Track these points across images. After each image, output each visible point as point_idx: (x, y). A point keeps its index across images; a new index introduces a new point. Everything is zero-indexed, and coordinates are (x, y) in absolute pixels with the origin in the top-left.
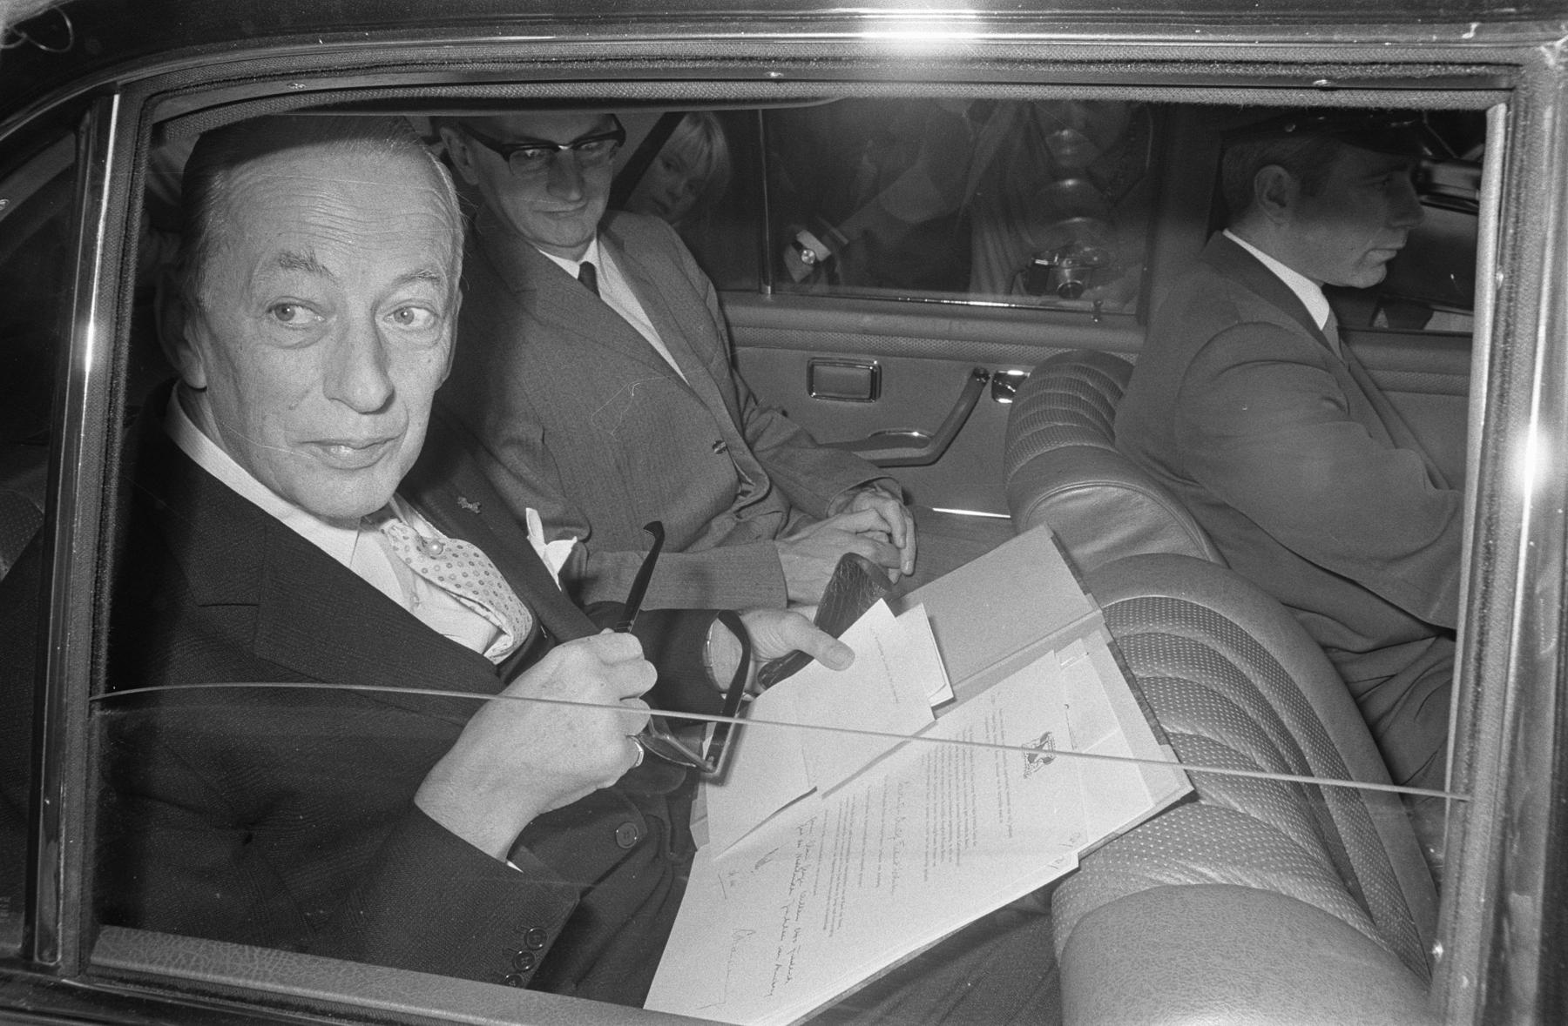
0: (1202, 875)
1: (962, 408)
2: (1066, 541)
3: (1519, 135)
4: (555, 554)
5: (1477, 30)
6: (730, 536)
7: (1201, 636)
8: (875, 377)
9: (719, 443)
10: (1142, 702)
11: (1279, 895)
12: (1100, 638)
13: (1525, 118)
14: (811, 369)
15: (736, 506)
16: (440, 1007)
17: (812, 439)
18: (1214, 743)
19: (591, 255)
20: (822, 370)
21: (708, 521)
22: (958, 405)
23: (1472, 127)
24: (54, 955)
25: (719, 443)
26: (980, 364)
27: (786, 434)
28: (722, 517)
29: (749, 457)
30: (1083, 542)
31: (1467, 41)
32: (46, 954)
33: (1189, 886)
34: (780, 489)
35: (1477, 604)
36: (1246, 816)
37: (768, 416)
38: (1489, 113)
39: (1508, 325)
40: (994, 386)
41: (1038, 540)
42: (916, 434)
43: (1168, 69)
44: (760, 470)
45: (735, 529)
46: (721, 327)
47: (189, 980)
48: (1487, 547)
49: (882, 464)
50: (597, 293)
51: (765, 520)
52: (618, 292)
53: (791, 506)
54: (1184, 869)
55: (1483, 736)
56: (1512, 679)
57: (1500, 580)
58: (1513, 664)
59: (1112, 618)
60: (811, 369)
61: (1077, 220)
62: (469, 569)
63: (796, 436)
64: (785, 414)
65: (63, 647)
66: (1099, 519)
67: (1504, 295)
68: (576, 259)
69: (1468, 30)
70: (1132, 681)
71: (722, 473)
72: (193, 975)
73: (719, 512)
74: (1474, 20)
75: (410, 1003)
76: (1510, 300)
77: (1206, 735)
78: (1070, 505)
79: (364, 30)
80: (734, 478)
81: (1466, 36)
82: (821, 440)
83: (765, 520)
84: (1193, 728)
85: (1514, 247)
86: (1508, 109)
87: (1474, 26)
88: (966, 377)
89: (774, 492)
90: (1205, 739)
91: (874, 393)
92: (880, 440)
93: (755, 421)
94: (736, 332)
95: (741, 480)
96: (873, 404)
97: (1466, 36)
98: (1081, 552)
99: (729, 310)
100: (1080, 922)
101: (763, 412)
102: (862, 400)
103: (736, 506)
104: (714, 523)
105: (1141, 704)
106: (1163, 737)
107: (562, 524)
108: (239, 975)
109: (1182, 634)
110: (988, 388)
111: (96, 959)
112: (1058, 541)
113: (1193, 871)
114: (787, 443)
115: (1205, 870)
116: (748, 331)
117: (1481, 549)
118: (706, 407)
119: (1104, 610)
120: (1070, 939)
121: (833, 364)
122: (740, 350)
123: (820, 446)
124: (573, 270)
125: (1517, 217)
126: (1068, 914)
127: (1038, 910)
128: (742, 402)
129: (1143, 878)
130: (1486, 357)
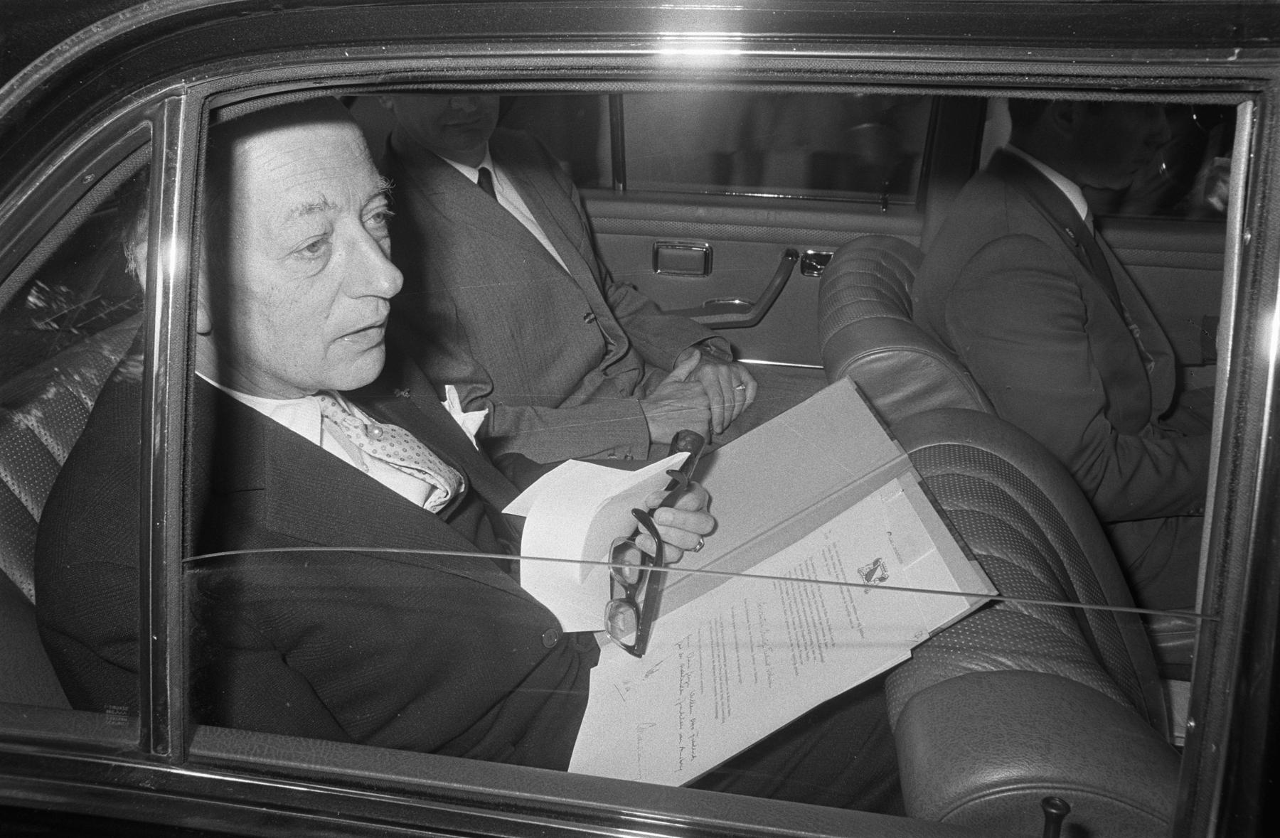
0: (1002, 664)
1: (778, 281)
2: (869, 393)
3: (1266, 132)
4: (470, 423)
5: (1240, 55)
6: (599, 389)
7: (986, 476)
8: (708, 257)
9: (588, 315)
10: (951, 528)
11: (1058, 677)
12: (911, 478)
13: (1272, 119)
14: (656, 254)
15: (603, 365)
16: (457, 782)
17: (658, 307)
18: (1003, 561)
19: (487, 165)
20: (665, 251)
21: (582, 379)
22: (775, 277)
23: (1228, 117)
24: (165, 749)
25: (588, 315)
26: (790, 246)
27: (638, 304)
28: (593, 374)
29: (613, 322)
30: (883, 394)
31: (1232, 63)
32: (160, 748)
33: (992, 672)
34: (636, 350)
35: (1228, 479)
36: (1030, 617)
37: (622, 290)
38: (1240, 108)
39: (1255, 275)
40: (803, 262)
41: (842, 391)
42: (737, 302)
43: (1003, 79)
44: (621, 333)
45: (603, 384)
46: (584, 220)
47: (265, 765)
48: (1236, 438)
49: (713, 327)
50: (495, 197)
51: (625, 376)
52: (508, 197)
53: (644, 362)
54: (987, 660)
55: (1231, 575)
56: (1253, 535)
57: (1245, 464)
58: (1254, 524)
59: (916, 461)
60: (656, 254)
61: (865, 126)
62: (406, 446)
63: (645, 305)
64: (635, 288)
65: (162, 523)
66: (894, 376)
67: (1253, 252)
68: (475, 167)
69: (1233, 54)
70: (941, 512)
71: (591, 339)
72: (268, 761)
73: (590, 369)
74: (1237, 46)
75: (435, 779)
76: (1257, 256)
77: (997, 555)
78: (874, 365)
79: (381, 45)
80: (602, 342)
81: (1231, 59)
82: (665, 308)
83: (625, 376)
84: (987, 550)
85: (1261, 217)
86: (1255, 105)
87: (1237, 51)
88: (780, 257)
89: (631, 353)
90: (997, 559)
91: (707, 270)
92: (713, 308)
93: (613, 295)
94: (595, 222)
95: (607, 343)
96: (707, 278)
97: (1231, 59)
98: (881, 402)
99: (592, 207)
100: (911, 699)
101: (617, 288)
102: (697, 275)
103: (603, 365)
104: (587, 379)
105: (950, 530)
106: (969, 555)
107: (472, 382)
108: (303, 761)
109: (972, 474)
110: (798, 266)
111: (193, 750)
112: (861, 390)
113: (995, 660)
114: (637, 312)
115: (1003, 660)
116: (606, 222)
117: (1232, 440)
118: (579, 287)
119: (910, 455)
120: (902, 713)
121: (673, 247)
122: (599, 236)
123: (663, 313)
124: (473, 176)
125: (1264, 192)
126: (899, 695)
127: (876, 687)
128: (603, 279)
129: (957, 666)
130: (1234, 293)
